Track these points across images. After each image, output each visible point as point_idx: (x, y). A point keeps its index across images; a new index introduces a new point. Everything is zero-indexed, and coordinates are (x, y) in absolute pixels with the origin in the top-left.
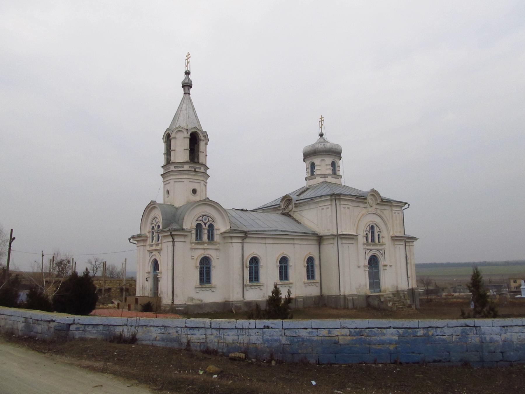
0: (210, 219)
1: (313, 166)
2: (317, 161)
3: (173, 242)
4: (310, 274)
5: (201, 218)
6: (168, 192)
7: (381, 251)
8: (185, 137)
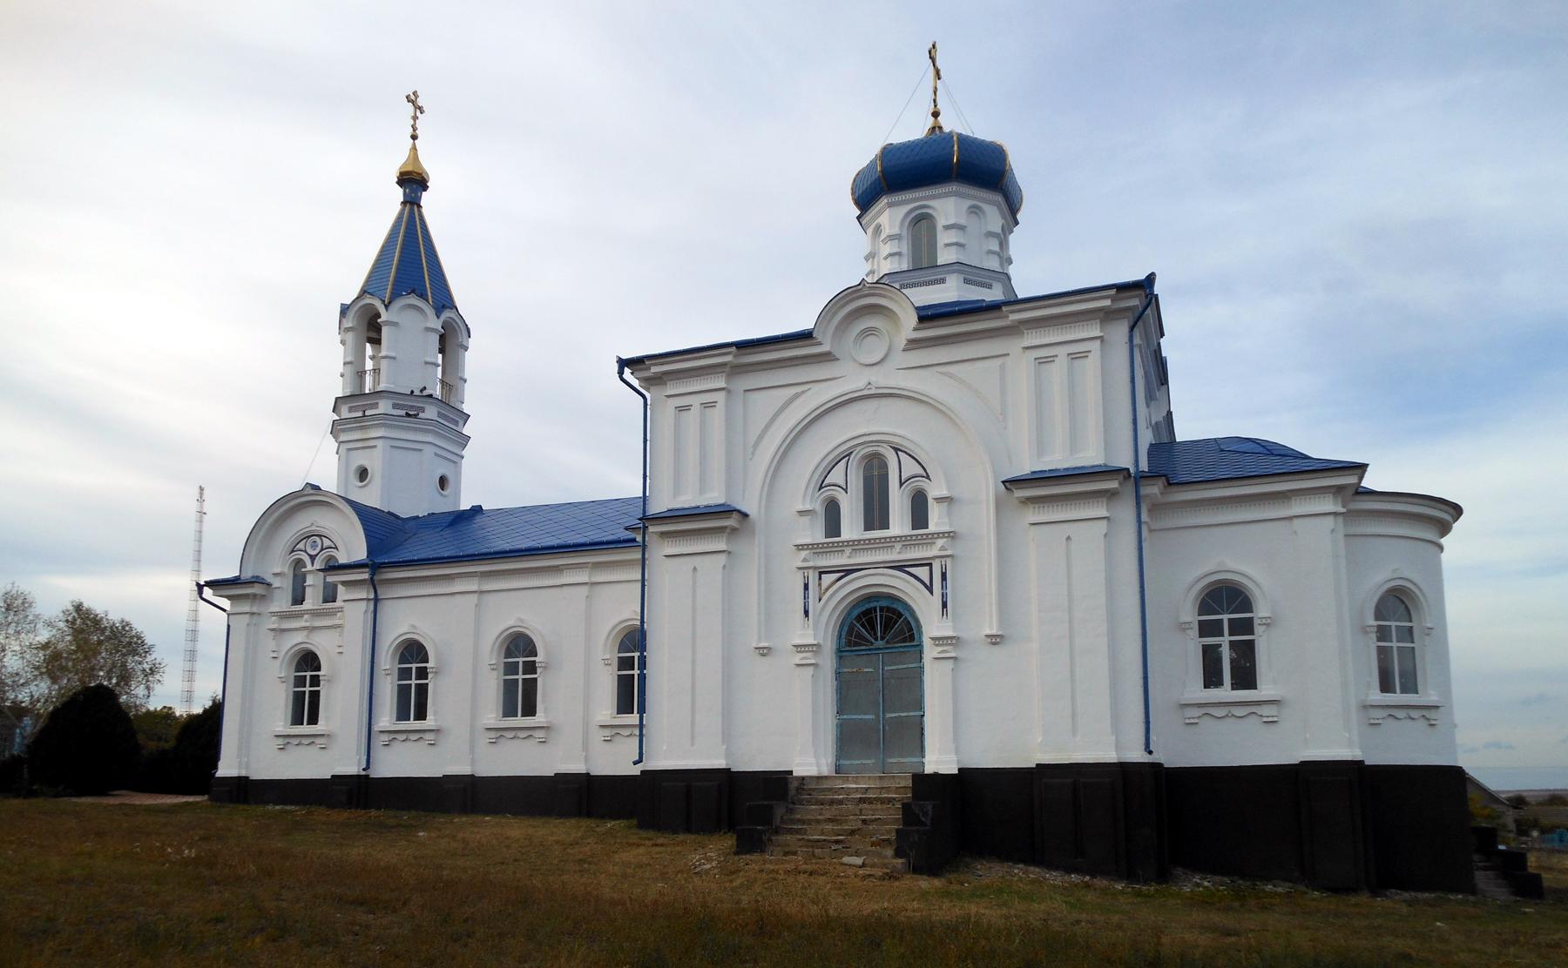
0: (327, 543)
1: (921, 223)
2: (948, 206)
3: (376, 600)
4: (630, 695)
5: (301, 546)
6: (363, 474)
7: (923, 572)
8: (428, 329)
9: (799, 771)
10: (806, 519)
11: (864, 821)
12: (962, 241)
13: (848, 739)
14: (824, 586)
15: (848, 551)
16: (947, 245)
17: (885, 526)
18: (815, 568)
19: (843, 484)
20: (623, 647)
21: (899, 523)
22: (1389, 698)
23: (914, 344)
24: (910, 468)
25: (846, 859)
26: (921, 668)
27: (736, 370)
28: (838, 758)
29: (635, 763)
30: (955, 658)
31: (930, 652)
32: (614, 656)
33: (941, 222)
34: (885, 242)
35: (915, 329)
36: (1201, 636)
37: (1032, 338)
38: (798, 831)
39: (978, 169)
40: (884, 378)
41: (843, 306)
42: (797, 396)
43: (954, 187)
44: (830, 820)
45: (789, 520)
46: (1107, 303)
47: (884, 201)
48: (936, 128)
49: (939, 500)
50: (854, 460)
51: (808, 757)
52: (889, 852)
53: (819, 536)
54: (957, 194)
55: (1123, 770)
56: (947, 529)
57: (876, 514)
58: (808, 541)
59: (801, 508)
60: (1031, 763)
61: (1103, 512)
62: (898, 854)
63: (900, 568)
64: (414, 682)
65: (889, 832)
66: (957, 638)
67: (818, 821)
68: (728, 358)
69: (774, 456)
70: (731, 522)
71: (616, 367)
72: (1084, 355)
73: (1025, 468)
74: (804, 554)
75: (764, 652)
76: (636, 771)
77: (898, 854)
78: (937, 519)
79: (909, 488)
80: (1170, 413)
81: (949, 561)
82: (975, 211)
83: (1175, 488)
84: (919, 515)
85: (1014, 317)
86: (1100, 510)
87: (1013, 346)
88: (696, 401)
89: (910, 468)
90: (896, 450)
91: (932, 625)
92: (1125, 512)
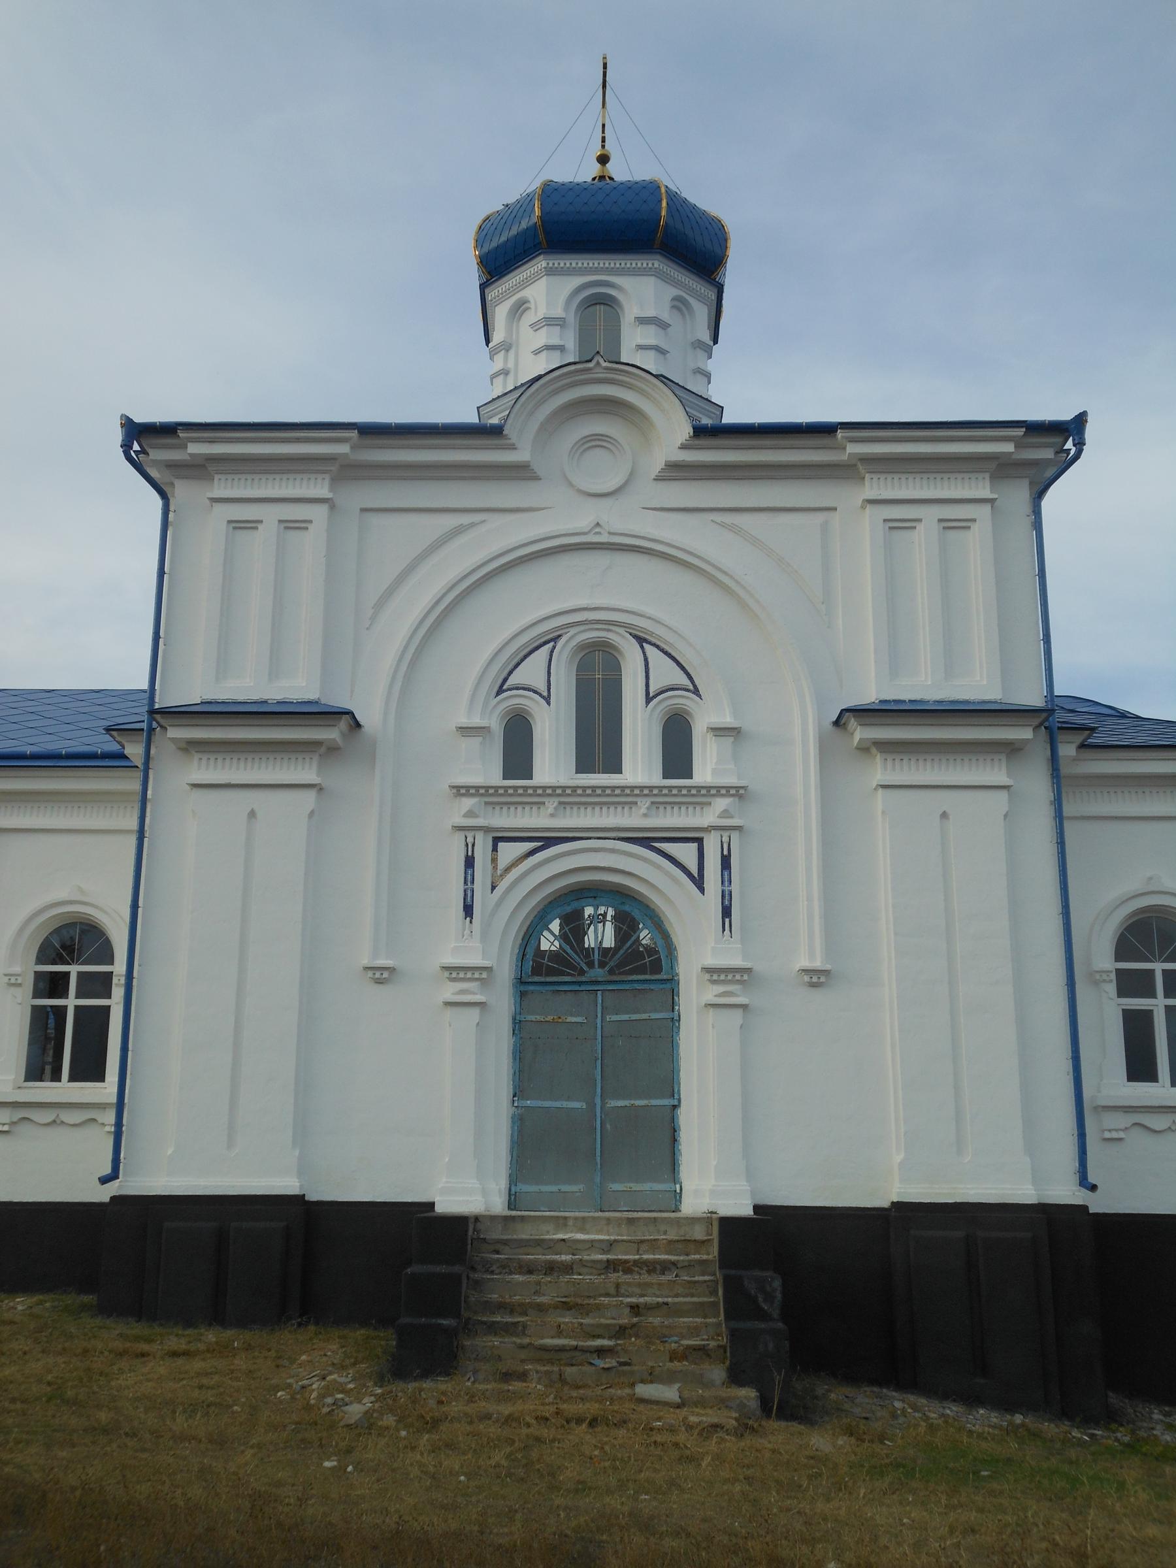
1: (599, 307)
2: (644, 291)
7: (686, 853)
9: (446, 1205)
10: (475, 742)
11: (635, 1309)
13: (535, 1145)
14: (503, 862)
15: (551, 804)
17: (618, 769)
18: (487, 830)
19: (542, 688)
20: (47, 953)
21: (640, 762)
22: (1143, 1092)
23: (675, 471)
24: (664, 673)
25: (642, 1390)
26: (674, 1022)
27: (346, 472)
28: (513, 1180)
29: (104, 1180)
30: (744, 1007)
31: (694, 994)
32: (27, 968)
33: (631, 310)
34: (535, 327)
35: (683, 447)
36: (1121, 994)
38: (509, 1329)
39: (691, 247)
40: (626, 519)
41: (556, 392)
42: (458, 531)
43: (656, 262)
44: (567, 1306)
45: (437, 737)
46: (1009, 448)
47: (541, 263)
49: (719, 731)
50: (564, 650)
51: (464, 1180)
52: (717, 1373)
53: (490, 772)
54: (658, 274)
55: (1050, 1219)
56: (731, 780)
57: (598, 745)
58: (478, 780)
59: (464, 721)
60: (881, 1199)
61: (1001, 778)
62: (736, 1377)
63: (645, 842)
64: (71, 1002)
65: (694, 1331)
66: (748, 970)
67: (541, 1308)
68: (343, 449)
69: (418, 627)
70: (330, 734)
71: (118, 436)
72: (964, 525)
73: (870, 695)
74: (468, 803)
75: (382, 976)
76: (103, 1194)
77: (736, 1377)
78: (708, 765)
79: (661, 706)
81: (735, 836)
82: (679, 305)
83: (1089, 754)
84: (677, 750)
85: (853, 449)
86: (995, 773)
87: (848, 497)
88: (270, 515)
89: (664, 673)
90: (641, 641)
91: (698, 943)
92: (1035, 784)
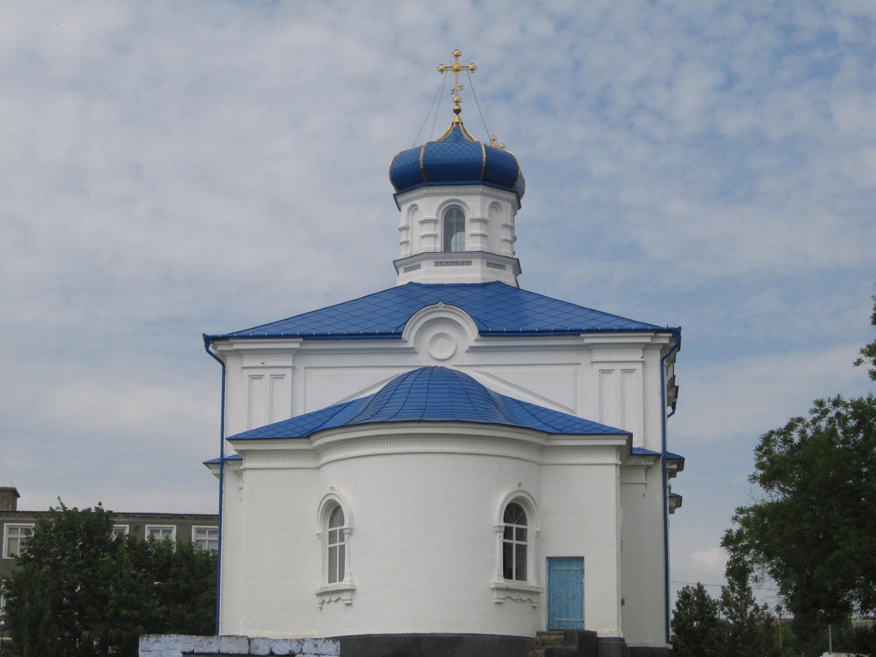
2: (475, 202)
12: (485, 232)
16: (472, 235)
23: (473, 350)
33: (468, 216)
37: (598, 356)
39: (499, 175)
42: (393, 416)
43: (480, 189)
48: (457, 133)
80: (674, 376)
82: (494, 206)
